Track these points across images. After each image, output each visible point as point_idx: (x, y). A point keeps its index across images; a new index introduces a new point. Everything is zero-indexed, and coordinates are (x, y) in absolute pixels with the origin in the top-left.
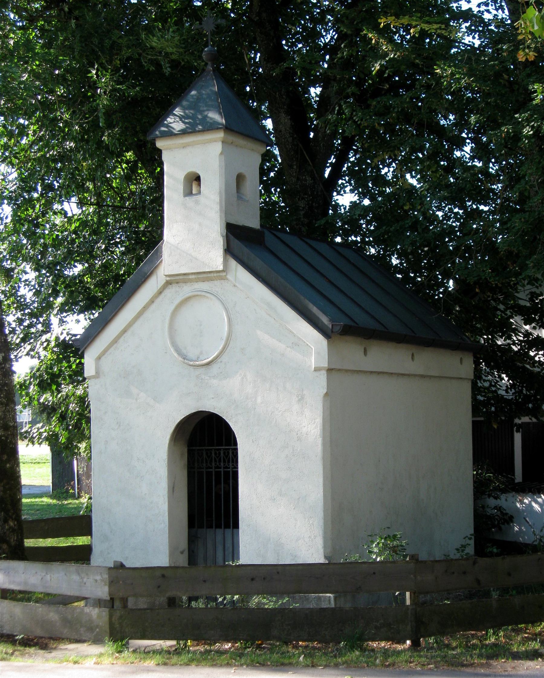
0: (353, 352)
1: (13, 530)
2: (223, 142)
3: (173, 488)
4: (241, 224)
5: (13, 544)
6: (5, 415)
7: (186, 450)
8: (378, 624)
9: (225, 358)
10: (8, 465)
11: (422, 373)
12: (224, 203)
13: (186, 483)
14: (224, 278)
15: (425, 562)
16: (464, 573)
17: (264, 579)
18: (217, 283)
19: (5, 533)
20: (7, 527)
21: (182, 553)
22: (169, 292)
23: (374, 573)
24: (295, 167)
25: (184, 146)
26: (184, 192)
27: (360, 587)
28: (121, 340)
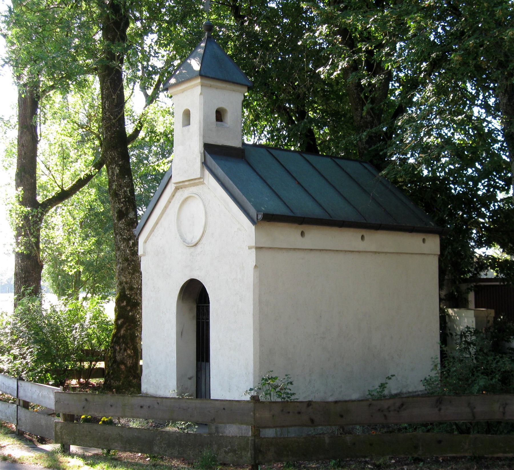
0: (287, 235)
1: (129, 356)
2: (201, 86)
3: (182, 333)
4: (221, 144)
5: (129, 365)
6: (131, 281)
7: (195, 306)
8: (227, 450)
9: (203, 241)
10: (130, 314)
11: (375, 250)
12: (202, 129)
13: (195, 330)
14: (203, 183)
15: (263, 402)
16: (299, 413)
17: (149, 407)
18: (201, 186)
19: (124, 358)
20: (125, 354)
21: (190, 379)
22: (178, 194)
23: (224, 409)
24: (359, 110)
25: (183, 91)
26: (183, 124)
27: (214, 419)
28: (156, 230)
